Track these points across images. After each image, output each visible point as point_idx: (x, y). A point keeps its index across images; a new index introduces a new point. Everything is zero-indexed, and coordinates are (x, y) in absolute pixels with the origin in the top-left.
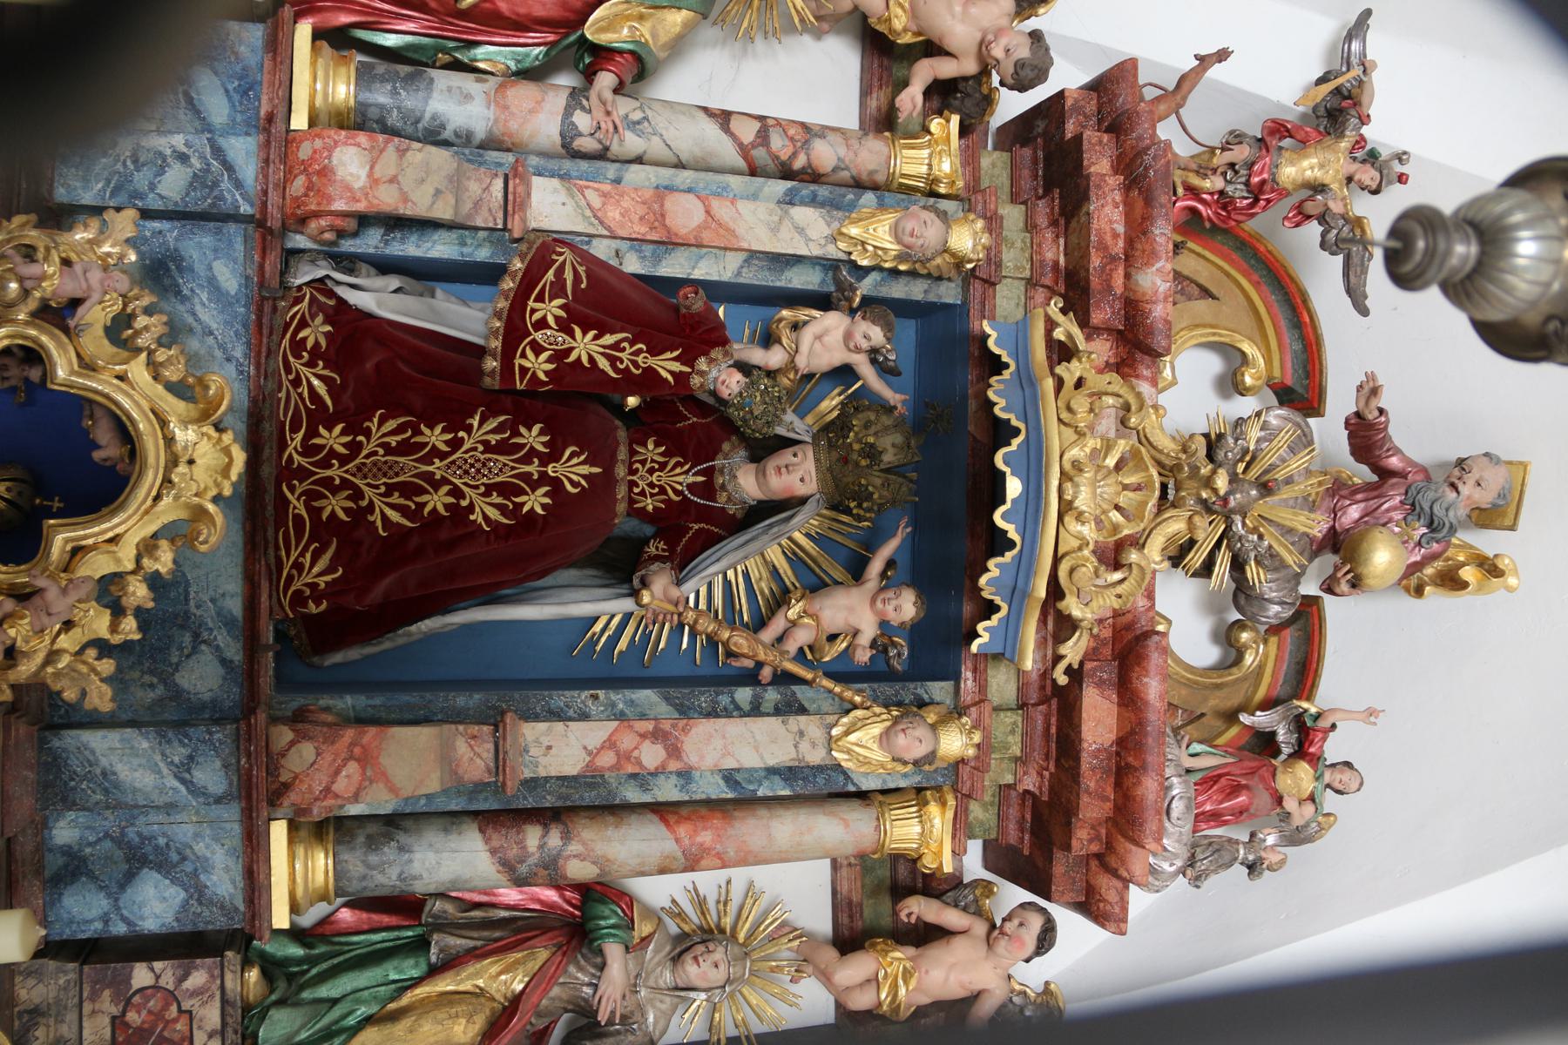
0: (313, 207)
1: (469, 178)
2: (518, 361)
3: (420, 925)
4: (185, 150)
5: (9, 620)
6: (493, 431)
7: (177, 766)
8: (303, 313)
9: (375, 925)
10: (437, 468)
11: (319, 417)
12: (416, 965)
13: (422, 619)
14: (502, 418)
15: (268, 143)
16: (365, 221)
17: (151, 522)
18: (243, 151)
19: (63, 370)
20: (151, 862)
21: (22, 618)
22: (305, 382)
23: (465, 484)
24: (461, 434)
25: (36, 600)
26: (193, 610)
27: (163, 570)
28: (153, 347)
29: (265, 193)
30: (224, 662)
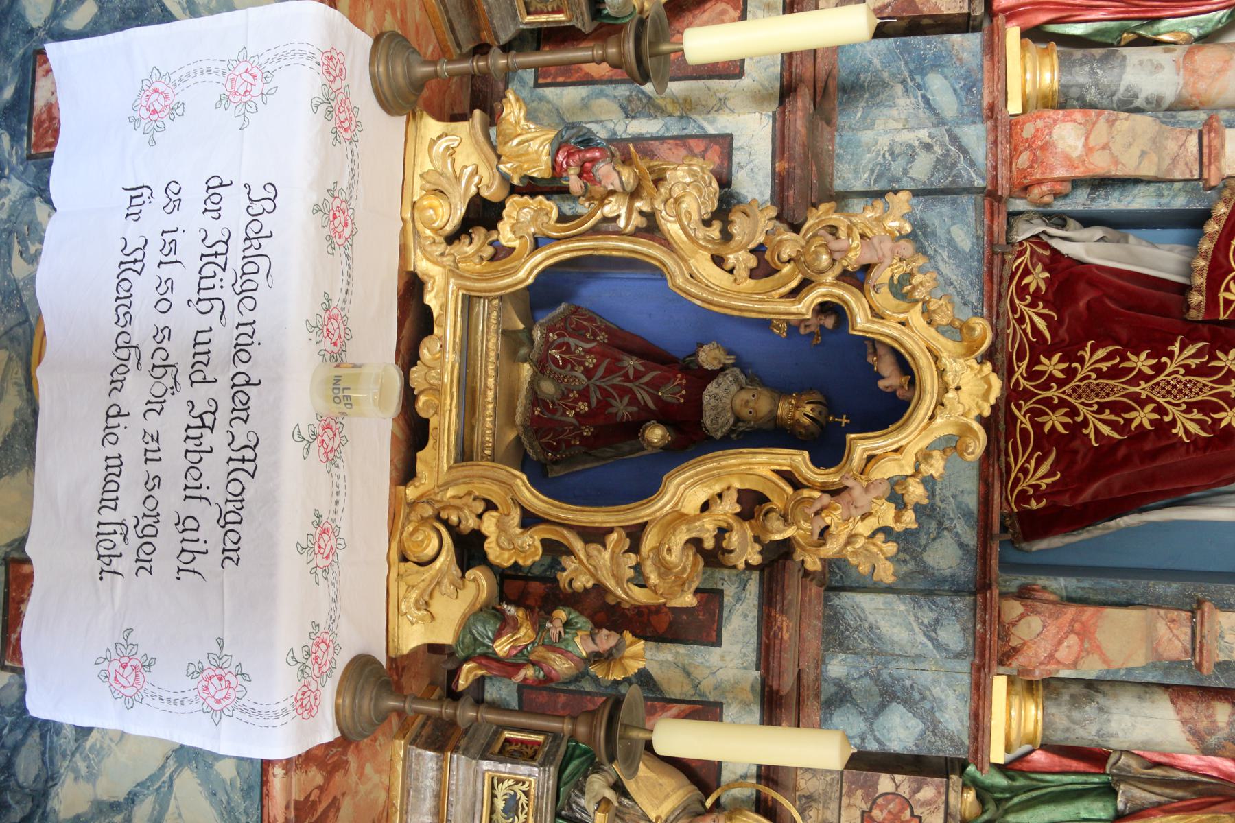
0: (1038, 176)
1: (1167, 138)
2: (1222, 295)
3: (1104, 774)
4: (929, 141)
5: (825, 511)
6: (1193, 356)
7: (926, 626)
8: (1026, 264)
9: (1067, 769)
10: (1143, 389)
11: (1039, 348)
12: (1105, 809)
13: (1121, 515)
14: (1200, 345)
15: (995, 127)
16: (1076, 183)
17: (927, 436)
18: (975, 136)
19: (862, 323)
20: (899, 698)
21: (836, 509)
22: (1028, 320)
23: (1168, 402)
24: (1164, 359)
25: (845, 495)
26: (938, 503)
27: (936, 475)
28: (927, 298)
29: (995, 168)
30: (961, 545)
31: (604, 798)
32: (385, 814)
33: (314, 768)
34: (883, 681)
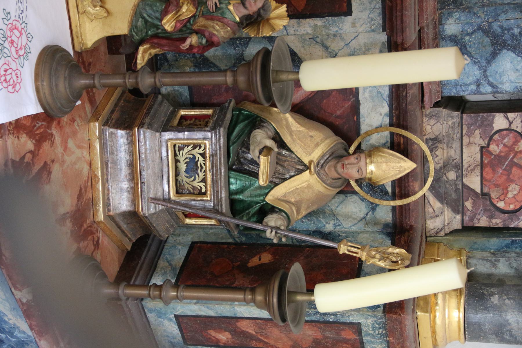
20: (508, 45)
31: (266, 147)
32: (89, 184)
33: (24, 135)
34: (494, 32)
